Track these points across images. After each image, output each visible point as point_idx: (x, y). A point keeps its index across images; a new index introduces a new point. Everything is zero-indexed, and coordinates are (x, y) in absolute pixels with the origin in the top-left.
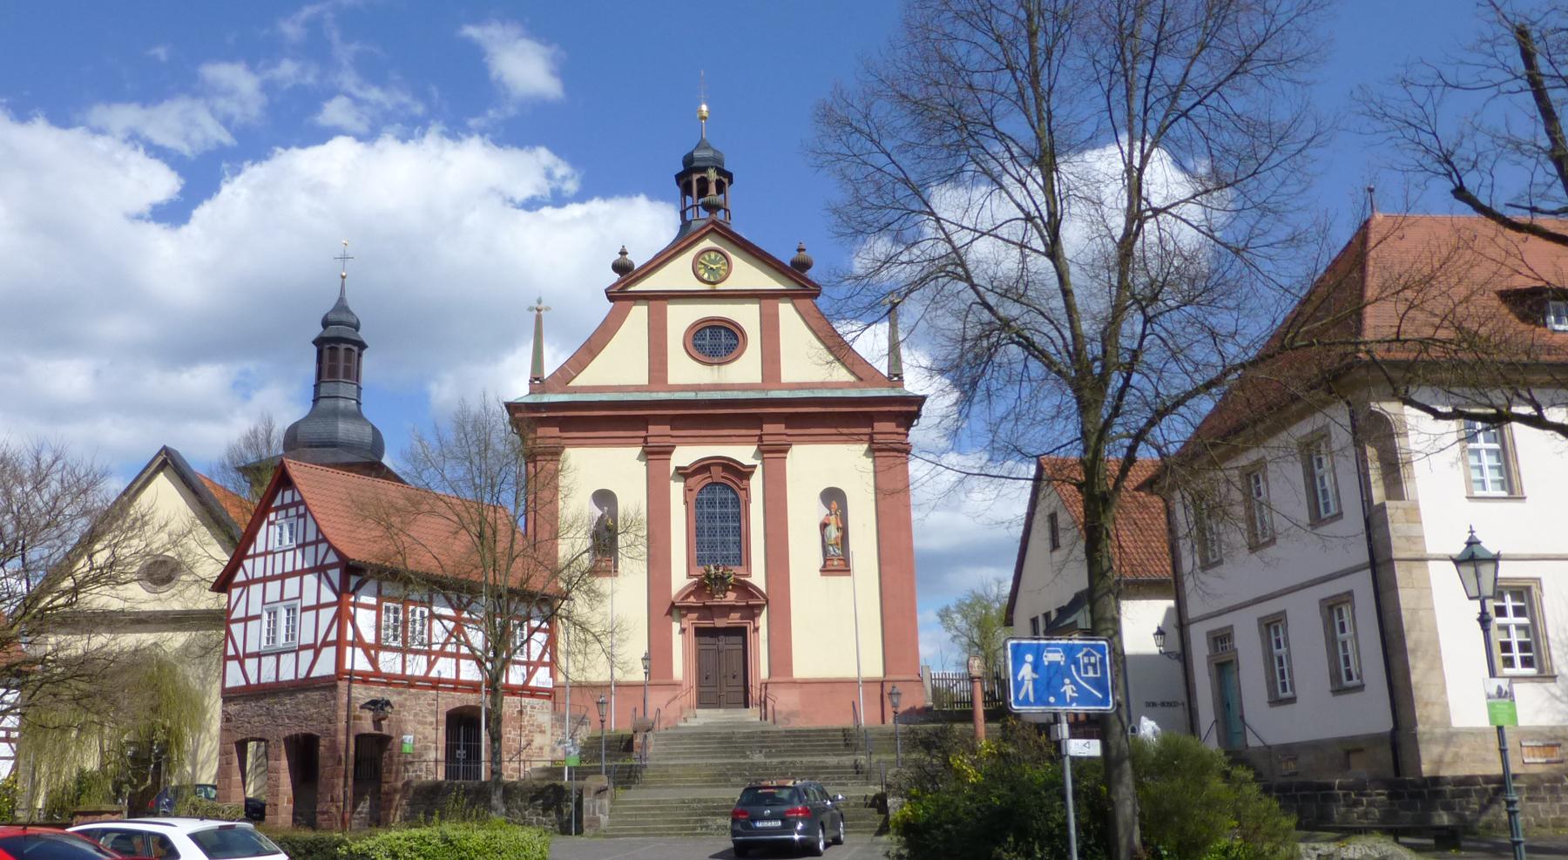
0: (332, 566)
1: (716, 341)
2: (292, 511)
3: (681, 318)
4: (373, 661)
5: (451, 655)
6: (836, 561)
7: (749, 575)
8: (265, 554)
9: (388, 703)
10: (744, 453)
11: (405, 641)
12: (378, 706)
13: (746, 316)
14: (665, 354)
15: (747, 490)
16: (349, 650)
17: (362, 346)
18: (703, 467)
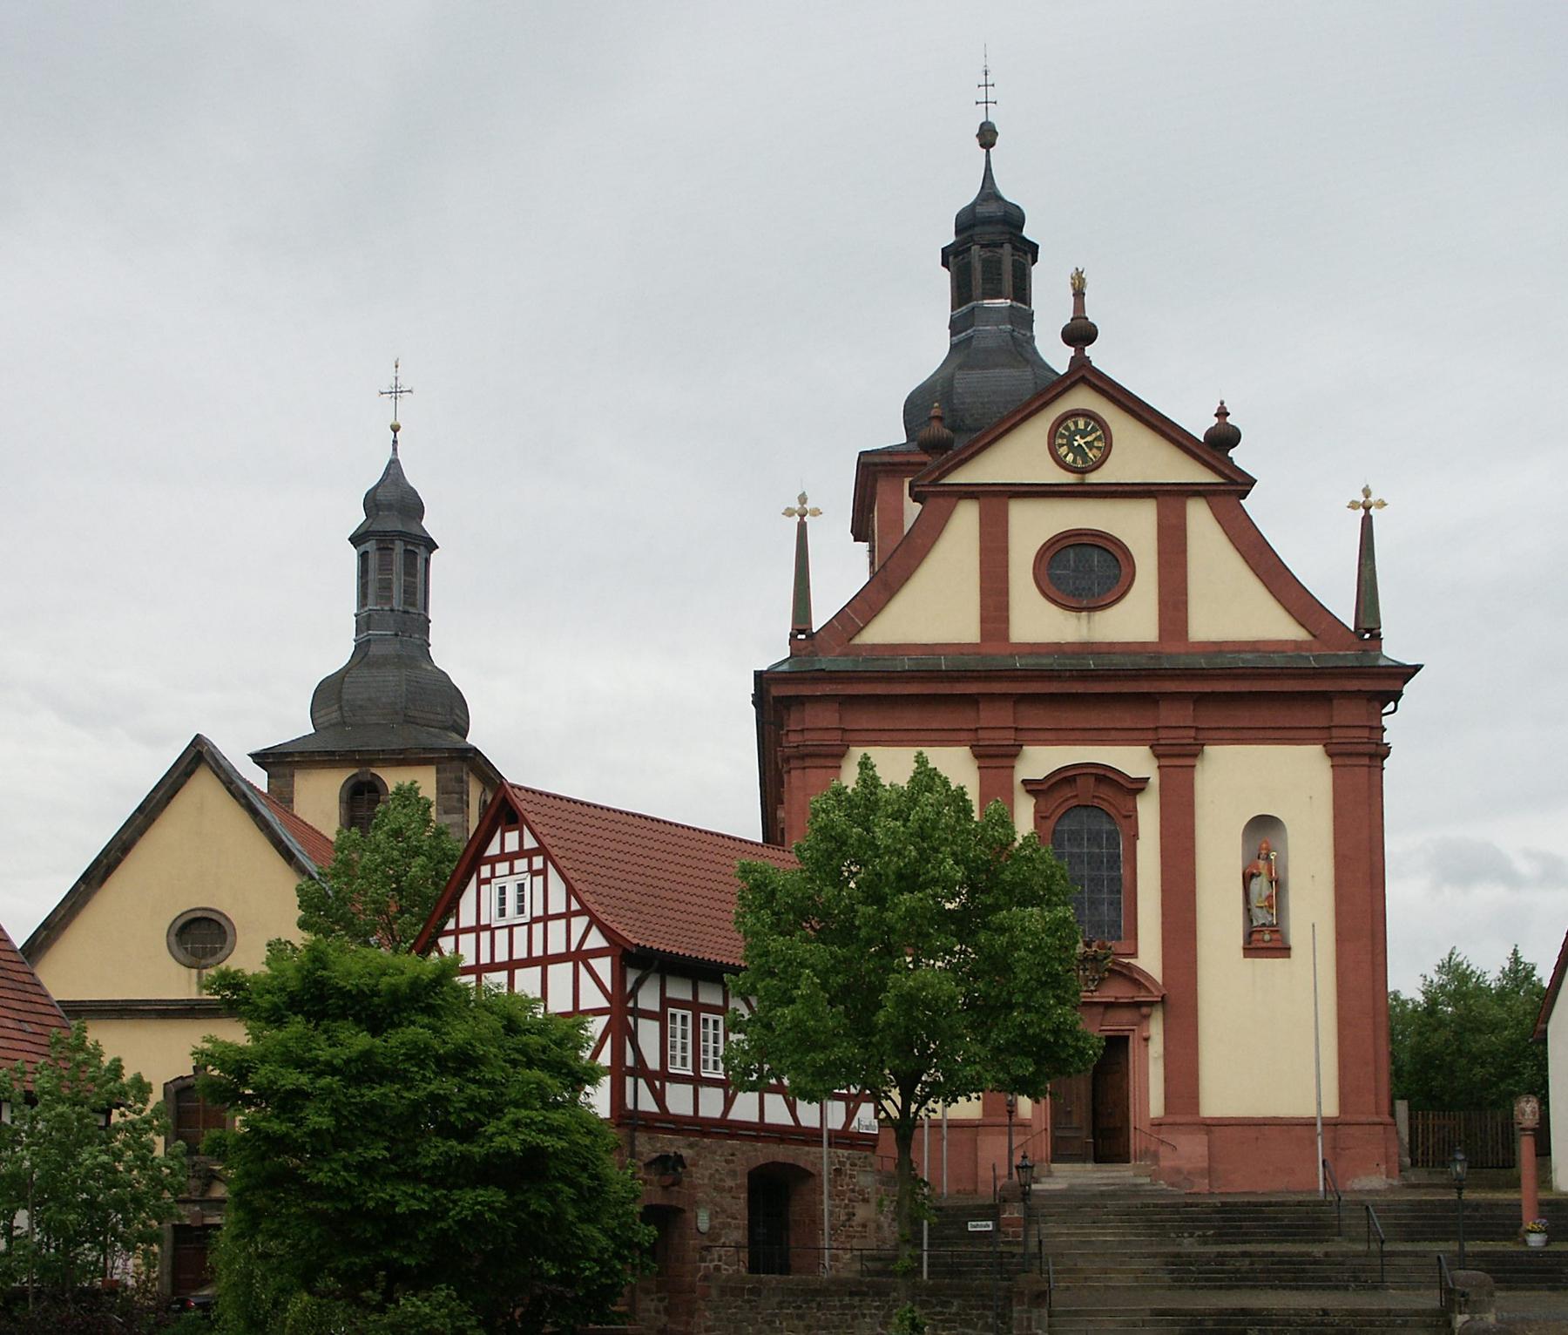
0: (597, 953)
1: (1086, 569)
2: (521, 865)
3: (1033, 527)
4: (659, 1097)
5: (752, 1088)
6: (1266, 940)
7: (1134, 955)
8: (478, 929)
9: (679, 1159)
10: (1133, 760)
11: (696, 1068)
12: (668, 1165)
13: (1134, 527)
14: (1005, 592)
15: (1132, 817)
16: (629, 1081)
17: (431, 546)
18: (1065, 778)
